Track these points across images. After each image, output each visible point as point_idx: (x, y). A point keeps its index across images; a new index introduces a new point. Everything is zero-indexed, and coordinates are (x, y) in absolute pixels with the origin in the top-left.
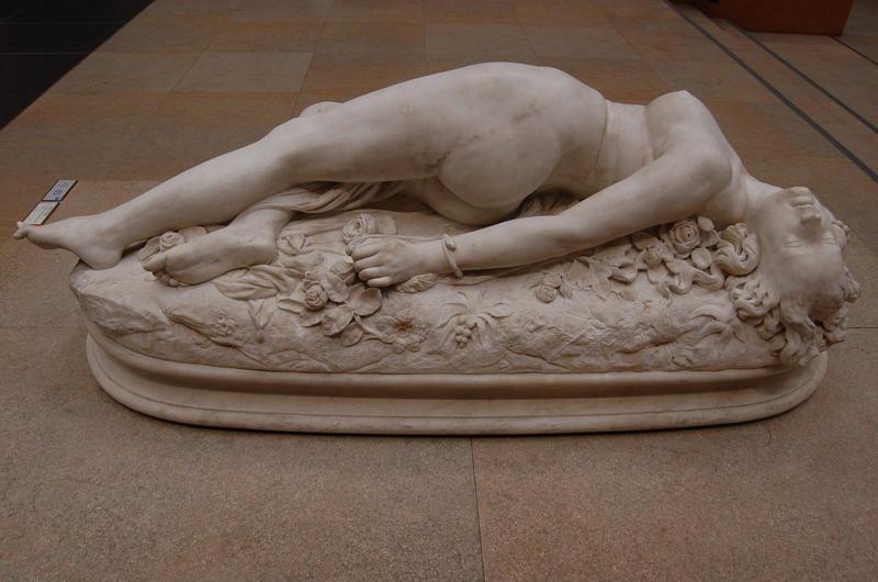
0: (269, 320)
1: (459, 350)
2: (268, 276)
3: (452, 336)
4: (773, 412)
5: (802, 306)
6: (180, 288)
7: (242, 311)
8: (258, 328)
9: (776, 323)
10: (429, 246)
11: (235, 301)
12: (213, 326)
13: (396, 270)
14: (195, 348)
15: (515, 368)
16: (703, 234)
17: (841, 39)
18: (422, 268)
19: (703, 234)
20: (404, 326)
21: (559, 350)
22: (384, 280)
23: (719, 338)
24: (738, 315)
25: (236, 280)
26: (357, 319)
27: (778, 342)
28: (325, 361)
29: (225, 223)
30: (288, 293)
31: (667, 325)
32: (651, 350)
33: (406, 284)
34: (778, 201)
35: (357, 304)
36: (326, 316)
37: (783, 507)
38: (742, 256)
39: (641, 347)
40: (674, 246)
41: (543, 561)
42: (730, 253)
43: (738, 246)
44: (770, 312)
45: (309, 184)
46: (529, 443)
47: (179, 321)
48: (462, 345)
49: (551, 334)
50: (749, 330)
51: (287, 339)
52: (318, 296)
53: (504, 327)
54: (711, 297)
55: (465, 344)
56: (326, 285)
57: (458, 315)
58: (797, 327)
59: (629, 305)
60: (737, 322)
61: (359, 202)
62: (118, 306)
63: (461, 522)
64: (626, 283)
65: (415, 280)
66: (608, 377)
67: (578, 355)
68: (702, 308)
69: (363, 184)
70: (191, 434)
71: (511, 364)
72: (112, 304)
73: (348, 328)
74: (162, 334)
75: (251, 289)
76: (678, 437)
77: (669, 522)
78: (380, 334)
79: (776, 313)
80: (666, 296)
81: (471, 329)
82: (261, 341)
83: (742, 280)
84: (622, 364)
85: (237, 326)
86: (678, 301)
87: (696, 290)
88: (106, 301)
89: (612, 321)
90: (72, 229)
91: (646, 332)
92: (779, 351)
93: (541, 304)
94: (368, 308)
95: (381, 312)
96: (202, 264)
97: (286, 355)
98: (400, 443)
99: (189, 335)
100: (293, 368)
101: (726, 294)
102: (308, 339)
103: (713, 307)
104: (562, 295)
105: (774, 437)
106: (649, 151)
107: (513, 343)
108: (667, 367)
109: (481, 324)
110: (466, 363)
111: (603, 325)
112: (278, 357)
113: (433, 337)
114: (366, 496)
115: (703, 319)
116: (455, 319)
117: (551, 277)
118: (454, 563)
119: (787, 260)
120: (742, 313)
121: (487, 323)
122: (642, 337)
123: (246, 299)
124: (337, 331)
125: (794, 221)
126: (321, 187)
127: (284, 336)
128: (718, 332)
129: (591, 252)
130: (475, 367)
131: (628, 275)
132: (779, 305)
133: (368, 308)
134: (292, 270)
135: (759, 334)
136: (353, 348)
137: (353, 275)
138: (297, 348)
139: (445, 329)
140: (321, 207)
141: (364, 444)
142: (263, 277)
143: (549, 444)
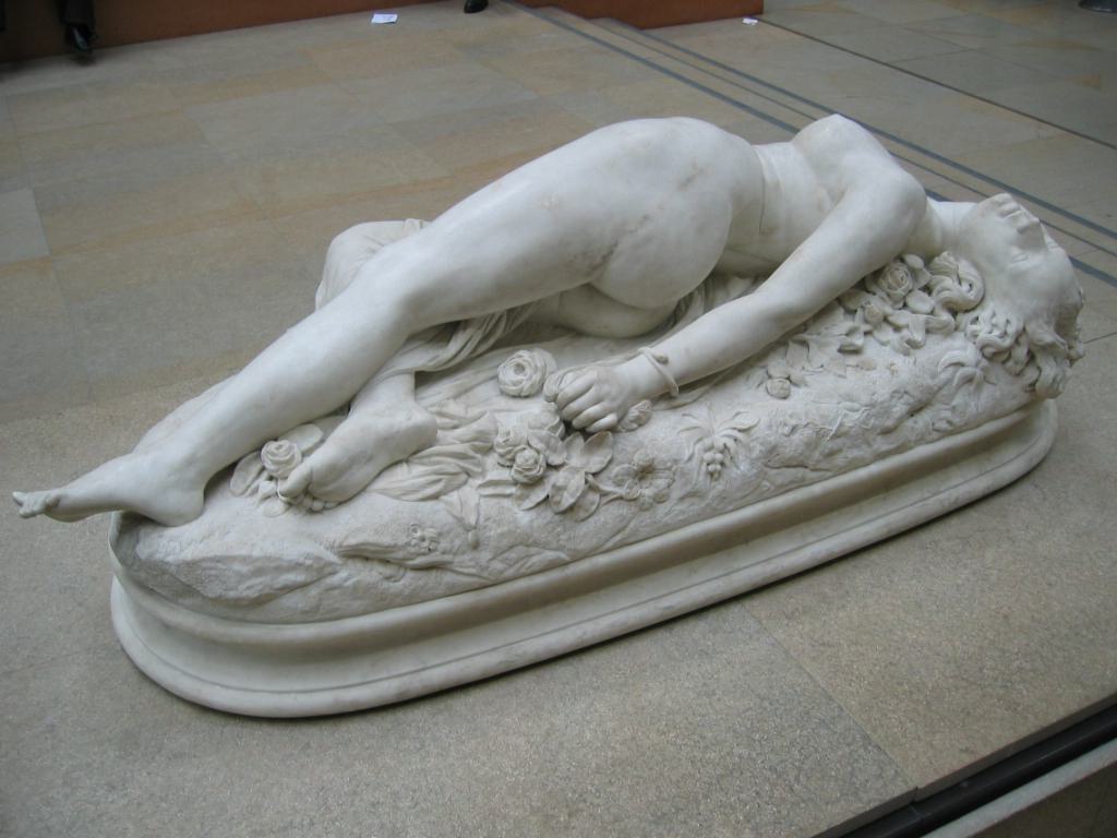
0: (479, 515)
1: (713, 484)
2: (449, 460)
3: (704, 467)
4: (1035, 462)
5: (1048, 323)
6: (326, 513)
7: (437, 514)
8: (468, 529)
9: (1025, 351)
10: (640, 366)
11: (422, 504)
12: (408, 544)
13: (618, 402)
14: (386, 584)
15: (781, 486)
16: (914, 273)
17: (764, 17)
18: (636, 395)
19: (914, 273)
20: (645, 472)
21: (820, 449)
22: (610, 419)
23: (972, 388)
24: (983, 355)
25: (405, 476)
27: (1031, 374)
28: (560, 548)
29: (344, 409)
30: (483, 474)
31: (922, 386)
32: (910, 423)
34: (983, 215)
35: (578, 461)
36: (554, 486)
37: (1100, 554)
38: (965, 287)
39: (901, 420)
40: (889, 295)
41: (911, 692)
42: (950, 288)
43: (955, 278)
44: (1017, 342)
45: (425, 331)
46: (805, 583)
47: (358, 554)
48: (716, 475)
49: (808, 432)
50: (998, 372)
51: (510, 531)
52: (536, 462)
53: (757, 439)
54: (949, 342)
55: (720, 473)
56: (540, 446)
57: (700, 440)
58: (1049, 349)
59: (873, 374)
60: (984, 363)
61: (492, 341)
62: (258, 559)
63: (798, 689)
64: (856, 351)
65: (634, 412)
66: (876, 468)
67: (840, 451)
68: (946, 357)
69: (493, 315)
70: (387, 721)
71: (773, 483)
72: (245, 560)
73: (583, 495)
74: (335, 579)
76: (954, 521)
77: (1006, 608)
78: (621, 491)
79: (1023, 340)
80: (906, 354)
81: (722, 452)
82: (476, 546)
83: (973, 315)
84: (885, 447)
85: (440, 534)
86: (922, 356)
87: (933, 338)
88: (234, 558)
89: (865, 399)
90: (119, 476)
91: (902, 401)
92: (1033, 385)
93: (781, 402)
94: (596, 461)
95: (615, 462)
97: (513, 555)
98: (662, 635)
99: (371, 570)
100: (523, 570)
101: (962, 334)
102: (535, 524)
103: (956, 353)
104: (796, 385)
105: (1045, 490)
106: (823, 193)
107: (772, 457)
108: (929, 438)
109: (731, 443)
110: (725, 498)
111: (856, 405)
112: (502, 561)
113: (683, 474)
114: (669, 704)
115: (951, 369)
116: (699, 446)
117: (777, 366)
118: (823, 732)
119: (1017, 278)
120: (989, 351)
122: (900, 408)
123: (435, 497)
124: (572, 501)
125: (1011, 232)
126: (446, 331)
127: (505, 529)
128: (969, 380)
129: (805, 327)
130: (736, 500)
131: (858, 341)
132: (1024, 329)
133: (596, 461)
134: (477, 443)
135: (1009, 372)
136: (591, 520)
137: (562, 427)
138: (526, 541)
139: (695, 462)
140: (450, 360)
141: (618, 651)
142: (438, 463)
143: (827, 577)
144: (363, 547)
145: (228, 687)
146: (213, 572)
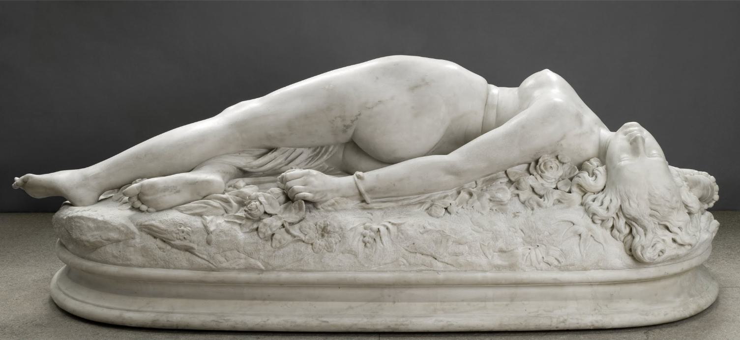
26: (286, 225)
33: (326, 204)
62: (100, 221)
75: (206, 207)
96: (167, 193)
121: (387, 228)
144: (150, 227)
145: (77, 300)
146: (78, 224)
